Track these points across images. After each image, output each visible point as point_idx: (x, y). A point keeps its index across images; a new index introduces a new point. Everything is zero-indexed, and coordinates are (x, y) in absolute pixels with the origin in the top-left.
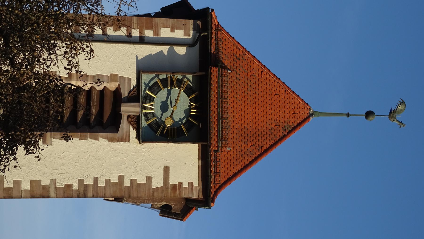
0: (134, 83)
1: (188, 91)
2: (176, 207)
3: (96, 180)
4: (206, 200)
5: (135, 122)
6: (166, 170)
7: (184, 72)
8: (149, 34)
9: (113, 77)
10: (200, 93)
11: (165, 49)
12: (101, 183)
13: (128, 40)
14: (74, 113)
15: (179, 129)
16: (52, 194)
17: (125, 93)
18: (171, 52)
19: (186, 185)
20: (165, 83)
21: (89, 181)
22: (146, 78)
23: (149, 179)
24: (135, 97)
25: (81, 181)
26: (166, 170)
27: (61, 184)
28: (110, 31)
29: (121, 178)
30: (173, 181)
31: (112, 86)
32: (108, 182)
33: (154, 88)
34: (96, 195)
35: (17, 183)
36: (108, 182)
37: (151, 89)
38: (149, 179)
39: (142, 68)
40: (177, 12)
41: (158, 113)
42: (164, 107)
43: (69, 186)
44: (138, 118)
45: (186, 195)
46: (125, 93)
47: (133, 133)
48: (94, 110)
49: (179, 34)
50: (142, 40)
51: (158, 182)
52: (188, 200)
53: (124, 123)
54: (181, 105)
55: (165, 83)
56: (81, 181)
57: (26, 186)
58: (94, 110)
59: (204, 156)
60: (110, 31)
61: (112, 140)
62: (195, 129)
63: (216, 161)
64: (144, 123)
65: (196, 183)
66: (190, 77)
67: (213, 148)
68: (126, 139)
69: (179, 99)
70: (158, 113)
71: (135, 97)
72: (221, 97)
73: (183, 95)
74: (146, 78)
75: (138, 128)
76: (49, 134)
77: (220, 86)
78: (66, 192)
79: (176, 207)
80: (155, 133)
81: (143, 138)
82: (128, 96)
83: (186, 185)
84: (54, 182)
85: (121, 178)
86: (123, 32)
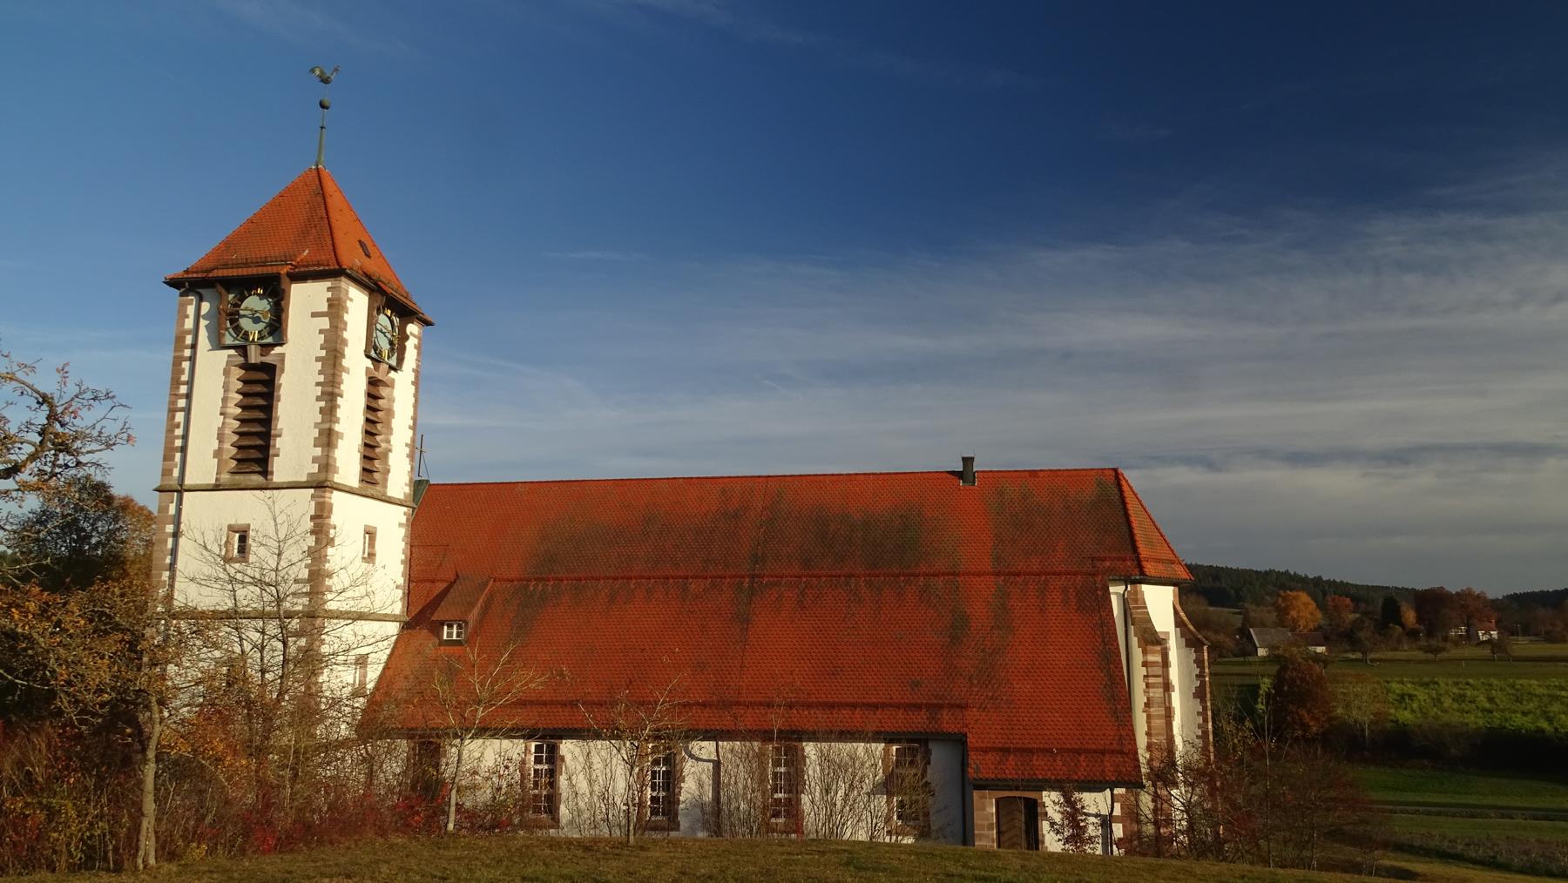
6: (314, 315)
9: (226, 372)
11: (203, 323)
13: (192, 359)
26: (314, 315)
27: (319, 418)
39: (218, 345)
47: (278, 350)
50: (194, 347)
53: (268, 359)
57: (318, 451)
64: (270, 340)
65: (328, 284)
74: (228, 340)
80: (276, 327)
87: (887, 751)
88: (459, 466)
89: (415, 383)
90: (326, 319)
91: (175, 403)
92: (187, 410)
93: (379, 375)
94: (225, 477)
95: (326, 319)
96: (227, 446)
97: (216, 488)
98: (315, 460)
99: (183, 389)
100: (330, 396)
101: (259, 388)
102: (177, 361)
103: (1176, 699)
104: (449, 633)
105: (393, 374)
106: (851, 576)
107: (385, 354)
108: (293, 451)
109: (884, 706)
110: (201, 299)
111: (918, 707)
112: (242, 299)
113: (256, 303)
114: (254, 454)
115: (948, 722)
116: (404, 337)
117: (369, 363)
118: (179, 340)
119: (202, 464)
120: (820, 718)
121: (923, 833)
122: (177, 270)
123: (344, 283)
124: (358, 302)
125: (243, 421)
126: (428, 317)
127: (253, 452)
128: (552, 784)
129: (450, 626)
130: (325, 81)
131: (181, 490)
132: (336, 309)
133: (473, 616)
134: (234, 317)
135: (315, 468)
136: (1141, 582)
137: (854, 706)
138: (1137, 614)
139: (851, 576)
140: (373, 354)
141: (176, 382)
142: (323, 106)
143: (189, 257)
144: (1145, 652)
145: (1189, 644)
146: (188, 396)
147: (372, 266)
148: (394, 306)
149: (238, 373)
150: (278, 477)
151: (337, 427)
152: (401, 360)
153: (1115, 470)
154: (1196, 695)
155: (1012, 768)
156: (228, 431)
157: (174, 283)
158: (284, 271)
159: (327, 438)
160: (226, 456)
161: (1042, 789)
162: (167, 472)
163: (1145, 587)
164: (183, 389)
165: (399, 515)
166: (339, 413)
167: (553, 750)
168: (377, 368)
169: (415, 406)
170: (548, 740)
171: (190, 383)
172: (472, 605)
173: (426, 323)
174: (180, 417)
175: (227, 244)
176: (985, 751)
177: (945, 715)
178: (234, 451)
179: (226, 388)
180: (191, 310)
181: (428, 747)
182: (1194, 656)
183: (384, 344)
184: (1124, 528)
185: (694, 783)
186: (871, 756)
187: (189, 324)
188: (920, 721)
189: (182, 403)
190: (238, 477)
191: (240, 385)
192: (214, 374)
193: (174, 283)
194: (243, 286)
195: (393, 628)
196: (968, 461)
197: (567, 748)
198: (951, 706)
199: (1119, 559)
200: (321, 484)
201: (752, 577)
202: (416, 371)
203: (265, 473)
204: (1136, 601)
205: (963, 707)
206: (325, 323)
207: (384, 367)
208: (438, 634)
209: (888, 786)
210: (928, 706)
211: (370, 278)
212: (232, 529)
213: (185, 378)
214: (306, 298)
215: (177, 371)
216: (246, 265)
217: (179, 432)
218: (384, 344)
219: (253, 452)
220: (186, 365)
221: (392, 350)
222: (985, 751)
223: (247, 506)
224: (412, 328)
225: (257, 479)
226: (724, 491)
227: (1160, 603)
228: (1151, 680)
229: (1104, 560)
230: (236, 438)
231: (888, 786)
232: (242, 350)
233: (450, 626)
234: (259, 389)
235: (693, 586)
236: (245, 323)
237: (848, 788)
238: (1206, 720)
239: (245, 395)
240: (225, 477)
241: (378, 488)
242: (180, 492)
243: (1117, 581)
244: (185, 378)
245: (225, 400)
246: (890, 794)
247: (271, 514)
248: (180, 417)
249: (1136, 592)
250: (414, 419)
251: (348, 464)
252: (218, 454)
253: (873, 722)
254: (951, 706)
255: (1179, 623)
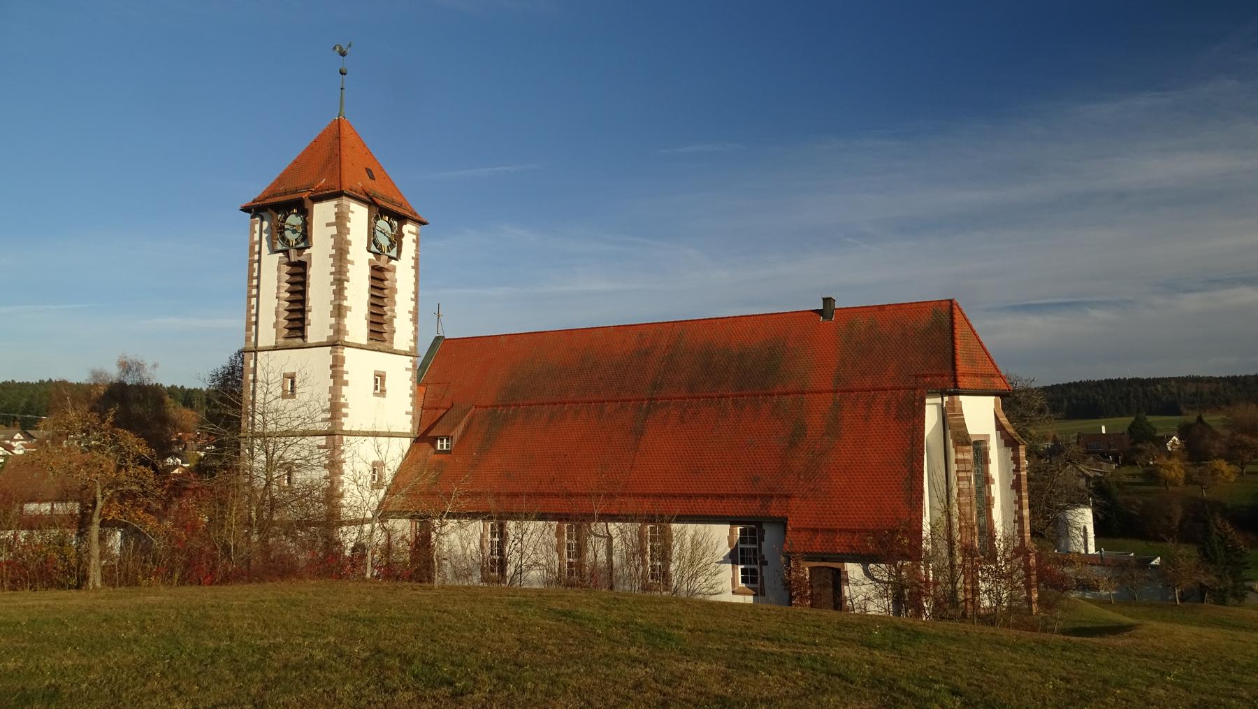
6: (328, 225)
9: (279, 269)
11: (265, 236)
13: (259, 261)
26: (328, 225)
27: (332, 297)
39: (273, 251)
44: (298, 249)
47: (307, 251)
50: (260, 253)
53: (302, 258)
57: (333, 321)
64: (302, 245)
65: (335, 202)
69: (369, 428)
74: (279, 247)
75: (304, 248)
80: (306, 236)
87: (731, 532)
88: (464, 324)
89: (416, 267)
90: (334, 228)
91: (250, 292)
92: (258, 296)
93: (381, 264)
94: (281, 341)
95: (334, 228)
96: (281, 319)
97: (275, 349)
98: (331, 327)
99: (255, 282)
100: (339, 281)
101: (299, 279)
102: (251, 263)
103: (996, 490)
104: (442, 445)
105: (393, 262)
106: (721, 397)
107: (385, 248)
108: (318, 324)
109: (728, 496)
110: (262, 220)
111: (755, 497)
112: (286, 218)
113: (294, 220)
114: (298, 324)
115: (775, 510)
116: (400, 235)
117: (372, 256)
118: (252, 248)
119: (267, 334)
120: (678, 507)
121: (759, 593)
122: (248, 200)
123: (345, 201)
124: (359, 214)
125: (291, 302)
126: (424, 218)
127: (296, 323)
128: (501, 552)
129: (442, 440)
130: (343, 54)
131: (256, 350)
132: (341, 220)
133: (457, 433)
134: (282, 230)
135: (331, 333)
136: (958, 394)
137: (706, 496)
138: (952, 420)
139: (721, 397)
140: (373, 248)
141: (251, 278)
142: (342, 73)
143: (254, 191)
144: (956, 452)
145: (1007, 444)
146: (258, 287)
147: (376, 187)
148: (387, 211)
149: (287, 269)
150: (311, 339)
151: (345, 303)
152: (399, 252)
153: (951, 301)
154: (1013, 487)
155: (818, 545)
156: (281, 309)
157: (246, 209)
158: (305, 196)
159: (339, 311)
160: (281, 327)
161: (843, 561)
162: (248, 339)
163: (962, 398)
164: (255, 282)
165: (407, 362)
166: (346, 293)
167: (502, 526)
168: (378, 259)
169: (416, 284)
170: (499, 520)
171: (258, 278)
172: (456, 425)
173: (421, 223)
174: (254, 301)
175: (280, 180)
176: (798, 530)
177: (774, 503)
178: (286, 322)
179: (279, 280)
180: (257, 227)
181: (424, 521)
182: (1011, 454)
183: (384, 242)
184: (949, 350)
185: (596, 552)
186: (720, 537)
187: (256, 237)
188: (754, 508)
189: (254, 292)
190: (289, 341)
191: (288, 277)
192: (272, 268)
193: (246, 209)
194: (285, 208)
195: (407, 443)
196: (828, 301)
197: (511, 525)
198: (780, 496)
199: (938, 375)
200: (336, 343)
201: (650, 399)
202: (416, 259)
203: (303, 337)
204: (953, 409)
205: (788, 497)
206: (334, 230)
207: (384, 258)
208: (434, 445)
209: (733, 558)
210: (762, 496)
211: (367, 194)
212: (286, 376)
213: (255, 274)
214: (323, 212)
215: (251, 270)
216: (286, 193)
217: (254, 311)
218: (384, 242)
219: (296, 323)
220: (256, 265)
221: (392, 246)
222: (798, 530)
223: (291, 360)
224: (408, 228)
225: (299, 341)
226: (641, 335)
227: (980, 414)
228: (961, 474)
229: (925, 377)
230: (287, 313)
231: (733, 558)
232: (286, 252)
233: (442, 440)
234: (298, 275)
235: (609, 408)
236: (288, 234)
237: (707, 556)
238: (1021, 508)
239: (291, 283)
240: (281, 341)
241: (387, 344)
242: (255, 352)
243: (933, 394)
244: (255, 274)
245: (278, 288)
246: (734, 563)
247: (310, 364)
248: (254, 301)
249: (953, 402)
250: (416, 293)
251: (357, 325)
252: (276, 325)
253: (631, 505)
254: (780, 496)
255: (999, 427)
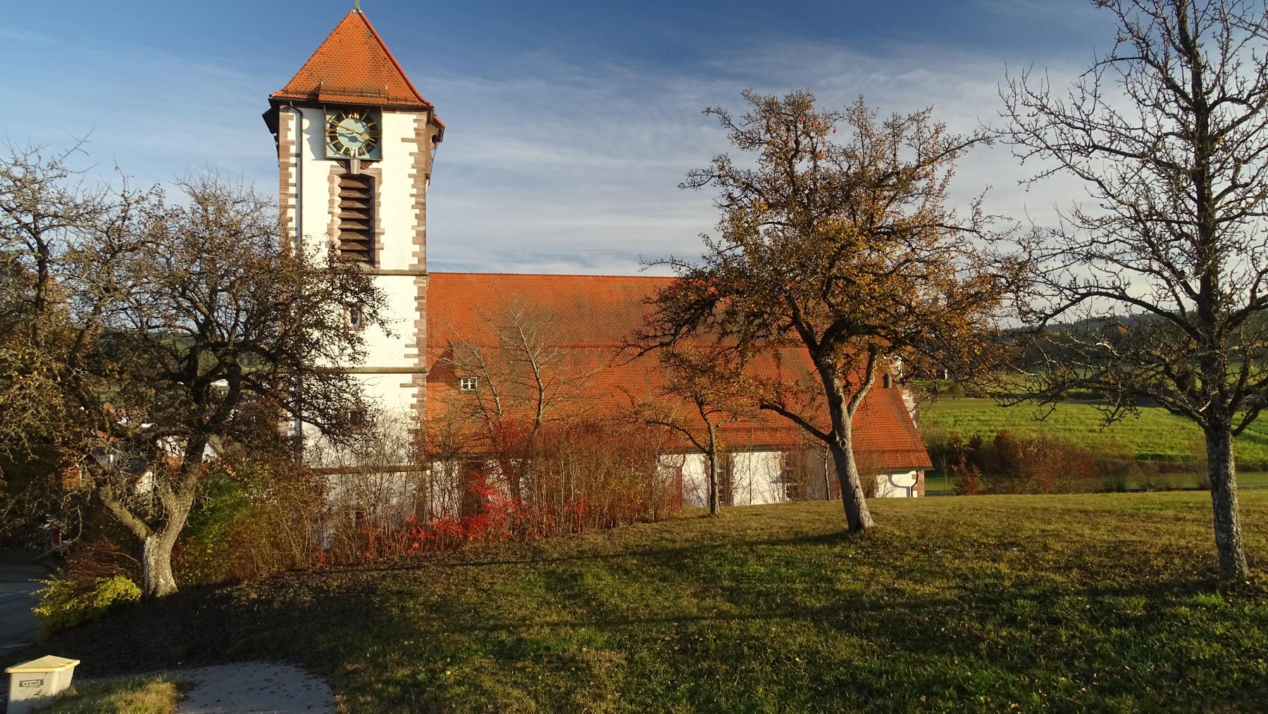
0: (335, 163)
1: (339, 119)
2: (435, 132)
3: (412, 195)
4: (427, 108)
5: (365, 163)
6: (404, 140)
7: (325, 122)
8: (293, 149)
9: (330, 179)
10: (342, 110)
11: (305, 137)
12: (415, 191)
13: (299, 166)
14: (358, 210)
15: (371, 128)
16: (422, 229)
17: (343, 171)
18: (308, 132)
19: (416, 125)
20: (333, 138)
21: (413, 201)
22: (330, 153)
23: (411, 154)
24: (346, 163)
25: (413, 207)
26: (404, 140)
27: (415, 222)
28: (293, 180)
29: (410, 176)
30: (412, 135)
31: (338, 180)
32: (413, 187)
33: (338, 147)
34: (424, 196)
35: (414, 254)
36: (413, 187)
37: (339, 150)
38: (411, 154)
40: (272, 120)
41: (359, 144)
42: (354, 139)
43: (417, 216)
44: (362, 161)
45: (423, 125)
46: (343, 171)
47: (375, 165)
48: (357, 195)
49: (292, 124)
50: (299, 155)
51: (414, 147)
52: (428, 122)
53: (367, 172)
54: (351, 126)
55: (333, 138)
56: (413, 207)
57: (417, 248)
58: (357, 195)
59: (392, 109)
60: (293, 180)
61: (381, 182)
62: (371, 115)
63: (397, 99)
64: (367, 157)
66: (328, 117)
67: (386, 102)
68: (379, 171)
70: (359, 144)
71: (346, 163)
72: (344, 92)
73: (342, 124)
74: (330, 153)
75: (371, 161)
76: (66, 482)
77: (335, 92)
78: (421, 218)
79: (435, 132)
80: (374, 144)
81: (379, 158)
82: (1207, 431)
83: (416, 125)
84: (413, 227)
85: (410, 176)
86: (293, 170)
